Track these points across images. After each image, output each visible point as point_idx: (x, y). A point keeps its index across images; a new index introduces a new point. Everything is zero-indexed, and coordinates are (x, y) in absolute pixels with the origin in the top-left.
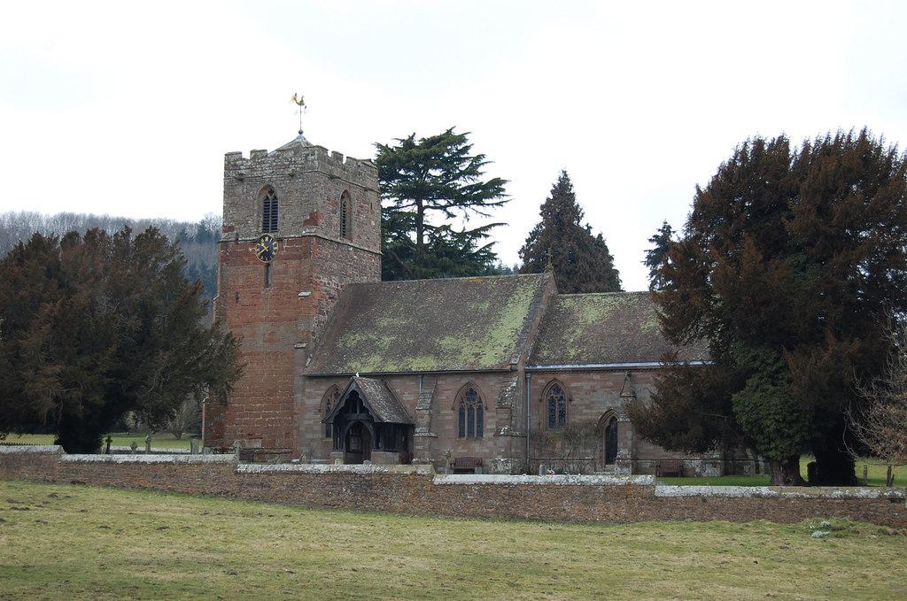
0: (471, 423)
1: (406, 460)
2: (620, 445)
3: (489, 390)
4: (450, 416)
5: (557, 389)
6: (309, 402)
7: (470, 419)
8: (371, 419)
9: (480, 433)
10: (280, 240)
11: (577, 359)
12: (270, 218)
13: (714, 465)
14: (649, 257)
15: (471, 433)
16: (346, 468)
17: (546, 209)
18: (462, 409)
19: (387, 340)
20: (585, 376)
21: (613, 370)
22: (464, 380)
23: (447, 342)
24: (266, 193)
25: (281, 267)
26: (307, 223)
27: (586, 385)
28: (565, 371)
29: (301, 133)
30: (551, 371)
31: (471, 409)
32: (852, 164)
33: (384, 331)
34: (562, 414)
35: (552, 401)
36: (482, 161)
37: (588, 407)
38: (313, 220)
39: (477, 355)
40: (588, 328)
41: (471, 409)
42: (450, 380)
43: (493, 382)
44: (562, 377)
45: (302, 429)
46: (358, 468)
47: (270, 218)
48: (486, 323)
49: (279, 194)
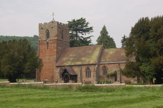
3: (92, 68)
5: (105, 67)
9: (90, 76)
15: (88, 76)
17: (101, 32)
19: (71, 59)
20: (110, 65)
23: (83, 59)
27: (111, 66)
28: (106, 64)
30: (104, 64)
31: (88, 72)
34: (106, 72)
39: (89, 61)
40: (111, 55)
42: (84, 66)
43: (92, 66)
44: (106, 65)
45: (56, 76)
47: (48, 36)
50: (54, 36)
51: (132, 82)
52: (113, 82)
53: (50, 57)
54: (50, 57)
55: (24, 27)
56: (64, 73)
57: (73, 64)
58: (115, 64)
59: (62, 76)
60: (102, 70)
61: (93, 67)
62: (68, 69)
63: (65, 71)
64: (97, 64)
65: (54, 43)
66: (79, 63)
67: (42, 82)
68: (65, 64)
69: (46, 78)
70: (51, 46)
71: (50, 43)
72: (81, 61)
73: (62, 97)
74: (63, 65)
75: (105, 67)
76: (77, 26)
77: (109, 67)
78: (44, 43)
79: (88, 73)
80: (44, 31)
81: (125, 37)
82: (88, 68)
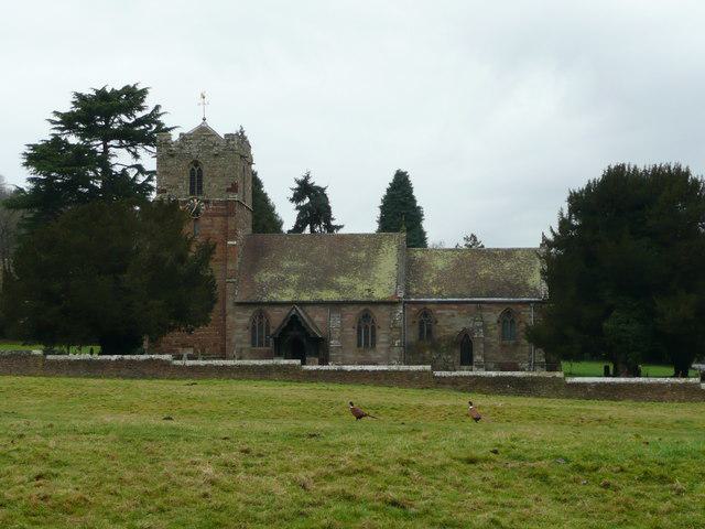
0: (366, 337)
1: (324, 362)
2: (475, 352)
3: (380, 314)
4: (351, 332)
5: (425, 314)
6: (241, 321)
7: (366, 334)
8: (307, 335)
9: (374, 344)
10: (207, 202)
11: (439, 294)
12: (196, 184)
14: (295, 195)
16: (403, 368)
18: (254, 328)
19: (294, 278)
20: (447, 306)
21: (467, 302)
22: (362, 308)
23: (342, 280)
24: (192, 166)
25: (207, 222)
26: (228, 190)
27: (448, 313)
28: (433, 303)
29: (204, 119)
31: (366, 327)
32: (669, 184)
33: (289, 270)
34: (429, 332)
35: (421, 323)
36: (160, 112)
37: (449, 327)
38: (234, 189)
39: (369, 290)
40: (440, 273)
42: (351, 308)
43: (384, 309)
44: (429, 307)
45: (233, 341)
46: (325, 367)
47: (196, 184)
48: (368, 267)
49: (205, 169)
50: (225, 187)
52: (457, 367)
57: (306, 298)
61: (388, 313)
64: (400, 302)
66: (332, 295)
67: (428, 367)
68: (274, 296)
70: (212, 226)
71: (206, 215)
72: (337, 288)
73: (273, 429)
74: (265, 299)
75: (426, 313)
76: (107, 116)
80: (183, 169)
81: (307, 177)
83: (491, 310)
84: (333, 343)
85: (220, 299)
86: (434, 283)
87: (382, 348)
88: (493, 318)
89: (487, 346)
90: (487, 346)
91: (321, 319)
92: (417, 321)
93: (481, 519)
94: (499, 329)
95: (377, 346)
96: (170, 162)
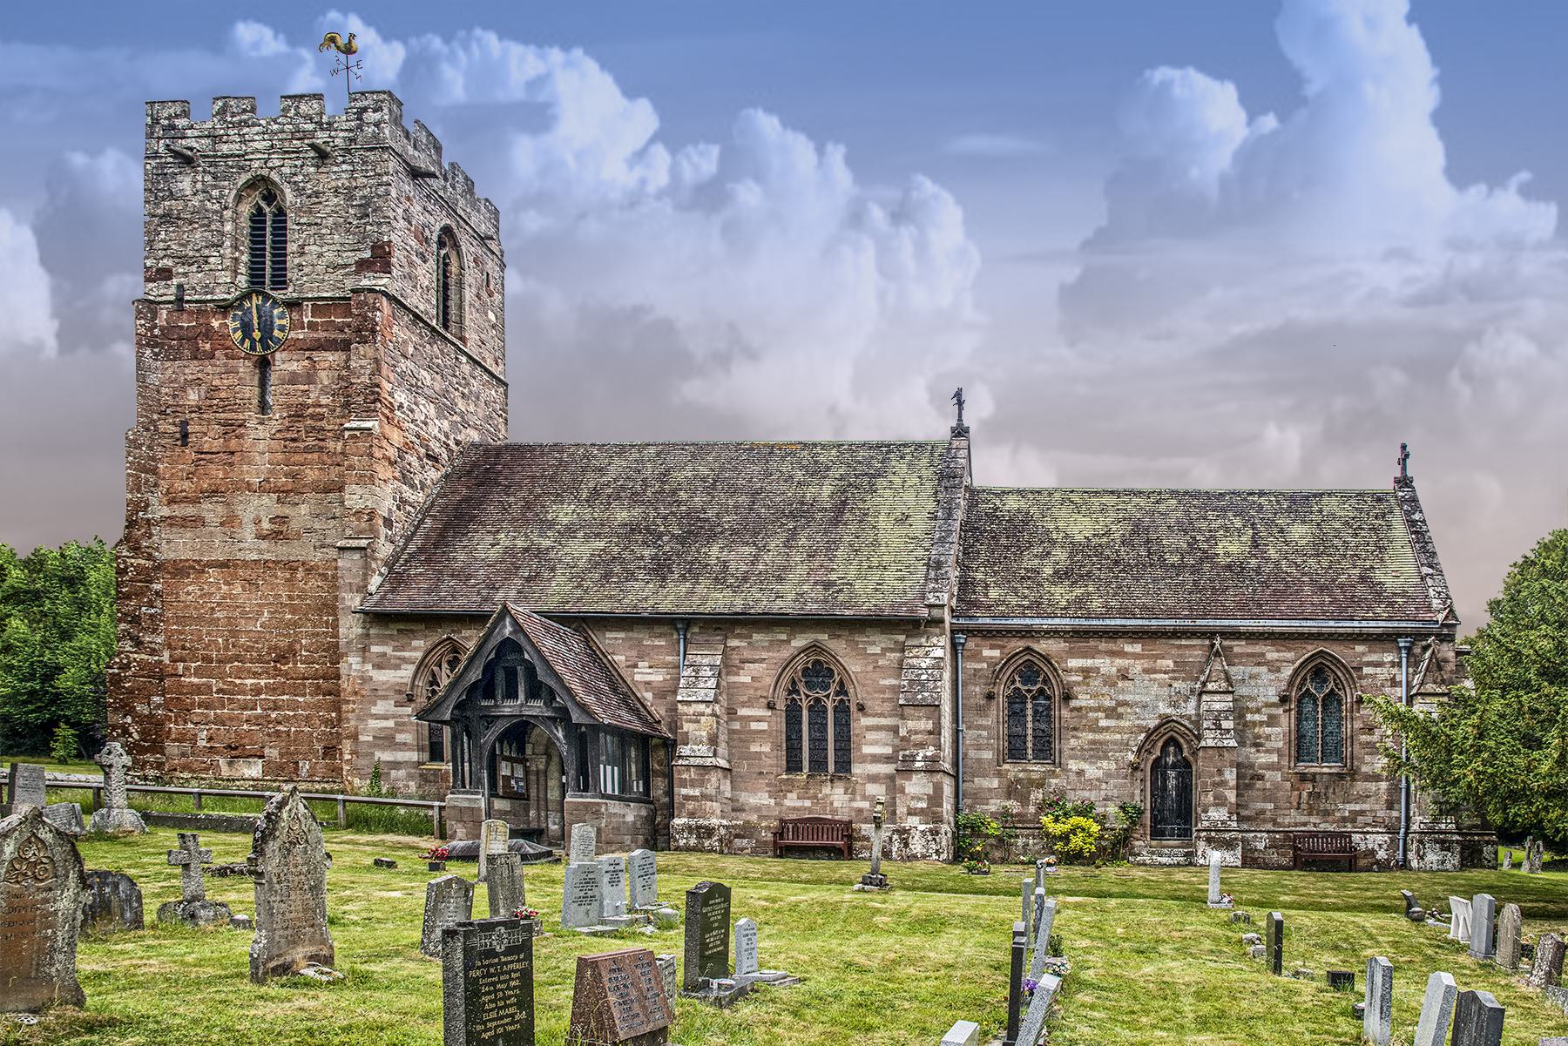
3: (864, 665)
4: (763, 722)
9: (844, 765)
10: (293, 305)
13: (1445, 846)
15: (818, 765)
26: (362, 266)
28: (1054, 633)
30: (1028, 633)
31: (817, 709)
33: (570, 531)
35: (1016, 699)
40: (1075, 548)
41: (817, 709)
43: (876, 644)
44: (1042, 646)
50: (351, 257)
51: (1372, 852)
53: (287, 511)
54: (287, 511)
55: (1435, 954)
56: (485, 688)
58: (1160, 646)
59: (455, 738)
60: (990, 697)
62: (559, 653)
63: (508, 666)
65: (345, 346)
66: (671, 598)
69: (236, 752)
75: (1032, 670)
77: (1086, 672)
78: (208, 334)
79: (818, 725)
82: (818, 671)
83: (1259, 660)
84: (694, 751)
85: (978, 880)
86: (1060, 576)
87: (873, 779)
88: (1266, 680)
89: (1248, 778)
90: (1248, 778)
91: (658, 677)
92: (1001, 690)
93: (336, 1041)
94: (1286, 722)
95: (857, 769)
96: (185, 184)
